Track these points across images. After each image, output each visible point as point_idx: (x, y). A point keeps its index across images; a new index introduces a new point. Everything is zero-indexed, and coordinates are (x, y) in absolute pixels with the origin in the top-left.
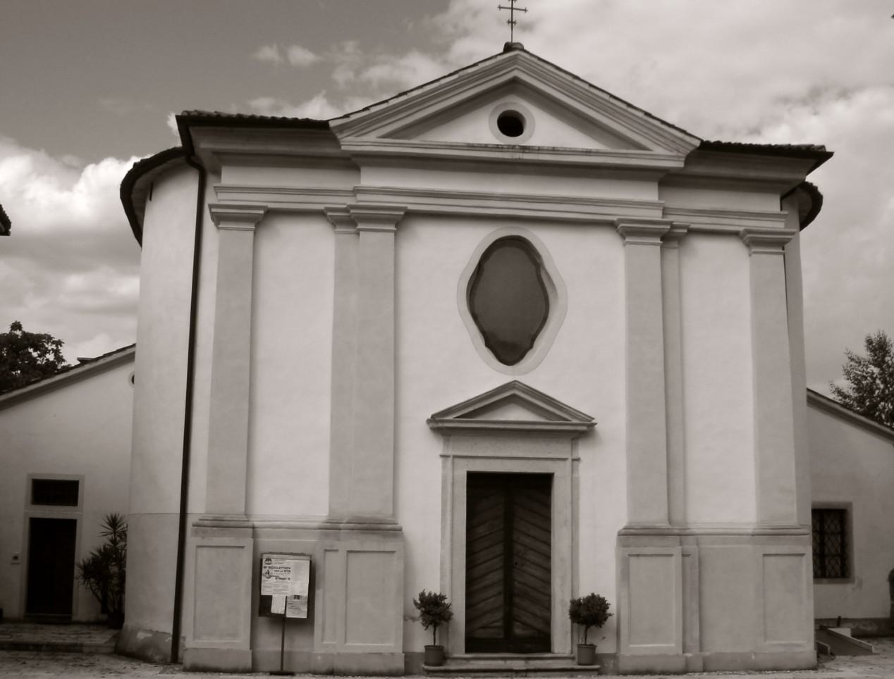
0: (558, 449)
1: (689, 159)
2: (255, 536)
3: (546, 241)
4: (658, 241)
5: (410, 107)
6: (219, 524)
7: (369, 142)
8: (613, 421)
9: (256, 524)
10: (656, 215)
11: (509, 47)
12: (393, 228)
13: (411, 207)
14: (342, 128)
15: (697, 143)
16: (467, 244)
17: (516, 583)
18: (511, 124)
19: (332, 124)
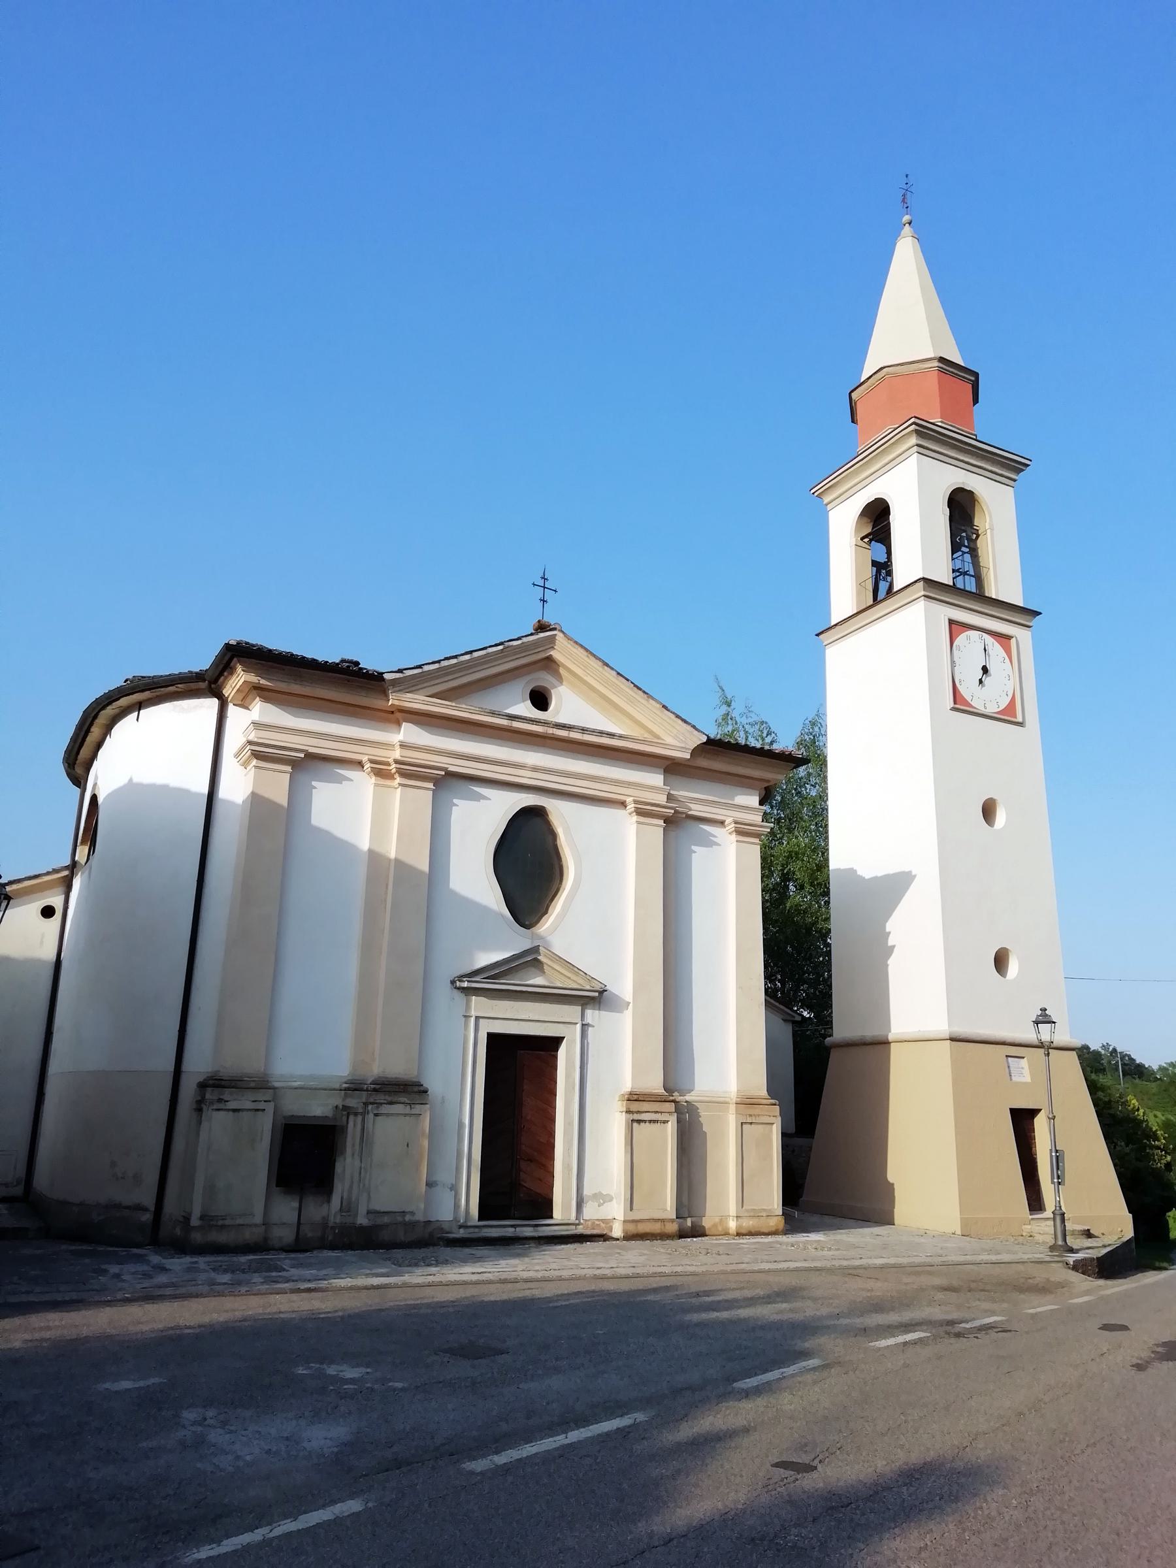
0: (571, 1012)
1: (698, 751)
2: (274, 1099)
3: (561, 814)
4: (661, 822)
5: (460, 670)
6: (217, 1086)
7: (416, 701)
8: (624, 986)
9: (276, 1084)
10: (662, 799)
11: (542, 627)
12: (431, 785)
13: (452, 768)
14: (394, 682)
15: (704, 739)
16: (500, 807)
17: (523, 1147)
18: (540, 700)
19: (387, 676)
